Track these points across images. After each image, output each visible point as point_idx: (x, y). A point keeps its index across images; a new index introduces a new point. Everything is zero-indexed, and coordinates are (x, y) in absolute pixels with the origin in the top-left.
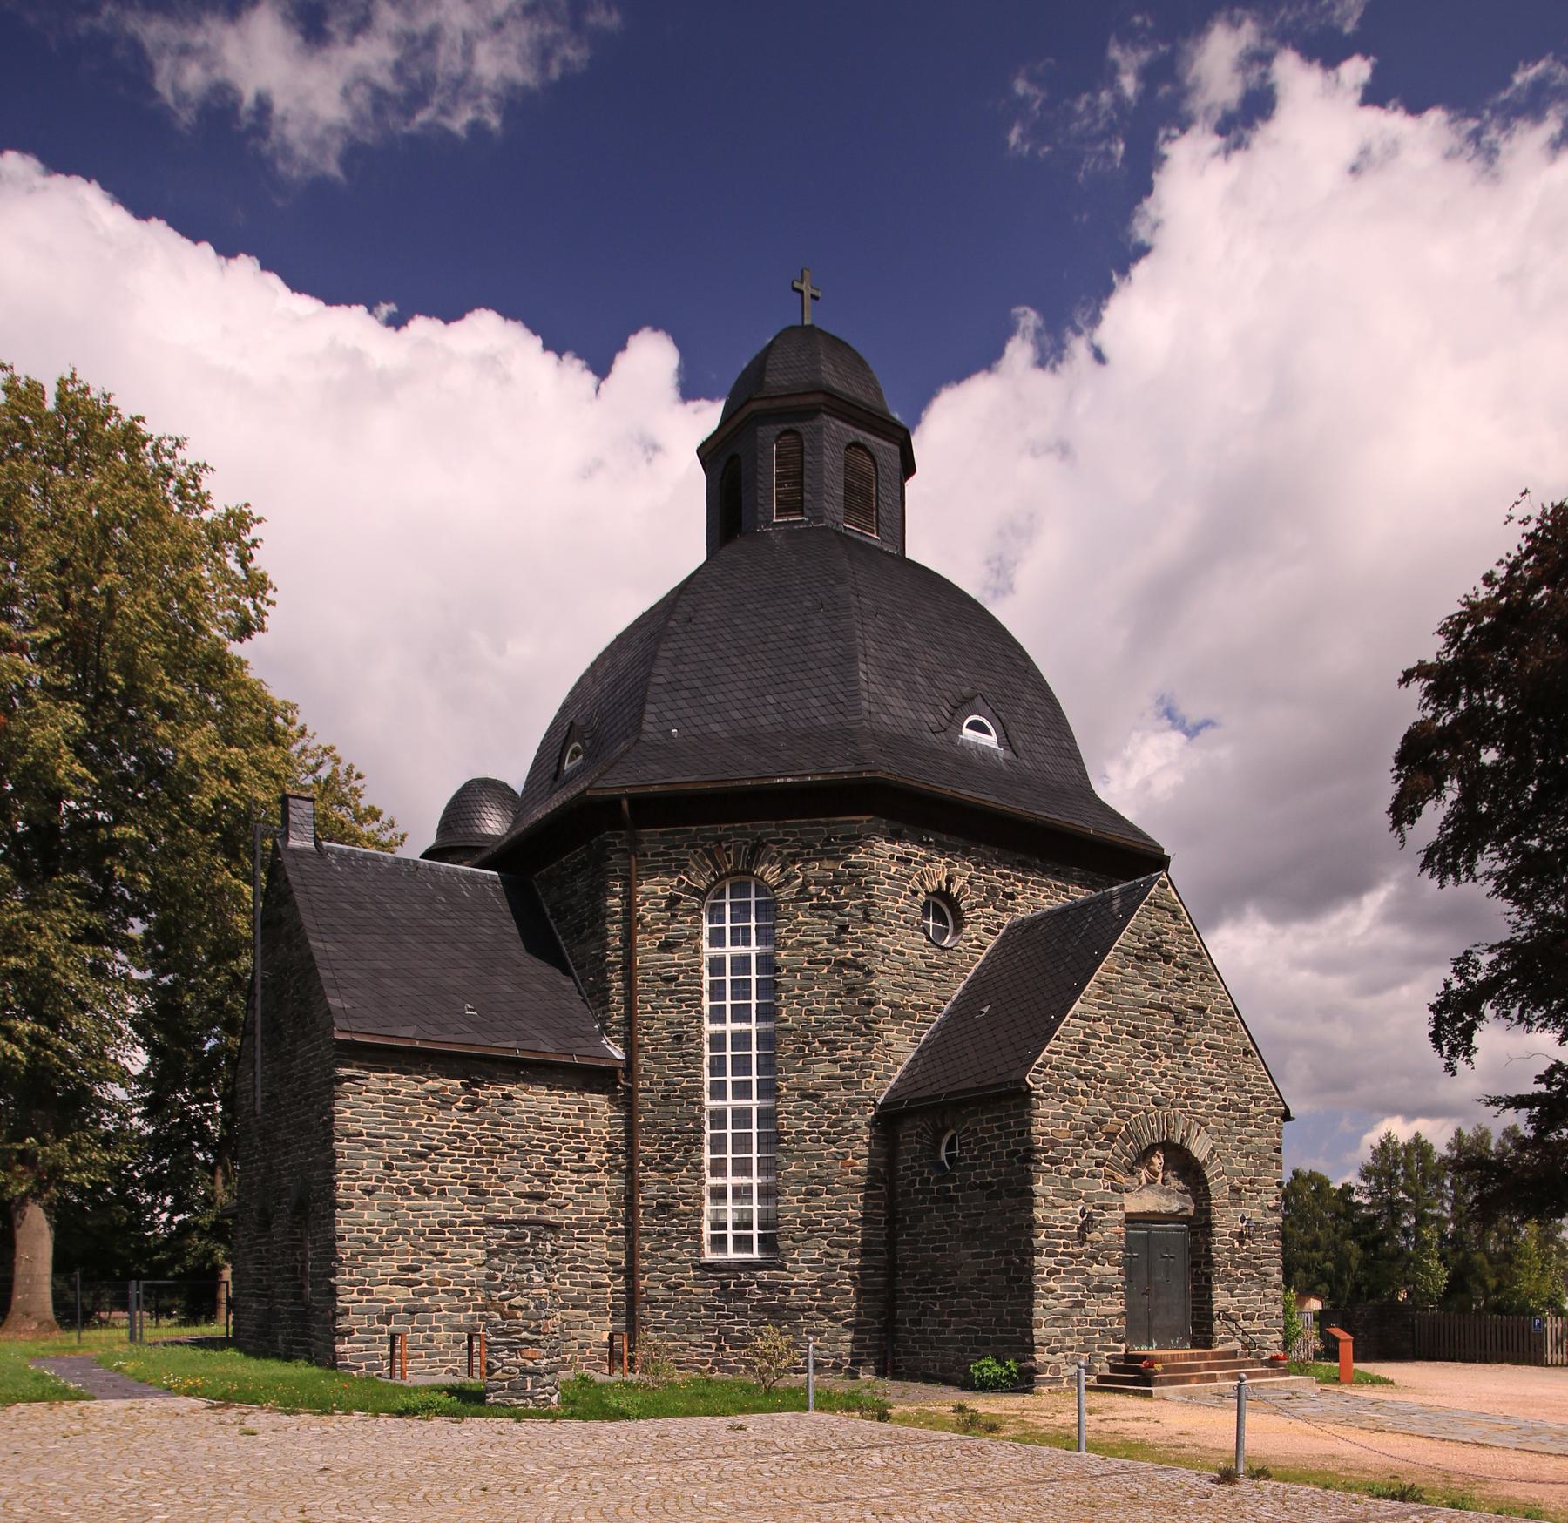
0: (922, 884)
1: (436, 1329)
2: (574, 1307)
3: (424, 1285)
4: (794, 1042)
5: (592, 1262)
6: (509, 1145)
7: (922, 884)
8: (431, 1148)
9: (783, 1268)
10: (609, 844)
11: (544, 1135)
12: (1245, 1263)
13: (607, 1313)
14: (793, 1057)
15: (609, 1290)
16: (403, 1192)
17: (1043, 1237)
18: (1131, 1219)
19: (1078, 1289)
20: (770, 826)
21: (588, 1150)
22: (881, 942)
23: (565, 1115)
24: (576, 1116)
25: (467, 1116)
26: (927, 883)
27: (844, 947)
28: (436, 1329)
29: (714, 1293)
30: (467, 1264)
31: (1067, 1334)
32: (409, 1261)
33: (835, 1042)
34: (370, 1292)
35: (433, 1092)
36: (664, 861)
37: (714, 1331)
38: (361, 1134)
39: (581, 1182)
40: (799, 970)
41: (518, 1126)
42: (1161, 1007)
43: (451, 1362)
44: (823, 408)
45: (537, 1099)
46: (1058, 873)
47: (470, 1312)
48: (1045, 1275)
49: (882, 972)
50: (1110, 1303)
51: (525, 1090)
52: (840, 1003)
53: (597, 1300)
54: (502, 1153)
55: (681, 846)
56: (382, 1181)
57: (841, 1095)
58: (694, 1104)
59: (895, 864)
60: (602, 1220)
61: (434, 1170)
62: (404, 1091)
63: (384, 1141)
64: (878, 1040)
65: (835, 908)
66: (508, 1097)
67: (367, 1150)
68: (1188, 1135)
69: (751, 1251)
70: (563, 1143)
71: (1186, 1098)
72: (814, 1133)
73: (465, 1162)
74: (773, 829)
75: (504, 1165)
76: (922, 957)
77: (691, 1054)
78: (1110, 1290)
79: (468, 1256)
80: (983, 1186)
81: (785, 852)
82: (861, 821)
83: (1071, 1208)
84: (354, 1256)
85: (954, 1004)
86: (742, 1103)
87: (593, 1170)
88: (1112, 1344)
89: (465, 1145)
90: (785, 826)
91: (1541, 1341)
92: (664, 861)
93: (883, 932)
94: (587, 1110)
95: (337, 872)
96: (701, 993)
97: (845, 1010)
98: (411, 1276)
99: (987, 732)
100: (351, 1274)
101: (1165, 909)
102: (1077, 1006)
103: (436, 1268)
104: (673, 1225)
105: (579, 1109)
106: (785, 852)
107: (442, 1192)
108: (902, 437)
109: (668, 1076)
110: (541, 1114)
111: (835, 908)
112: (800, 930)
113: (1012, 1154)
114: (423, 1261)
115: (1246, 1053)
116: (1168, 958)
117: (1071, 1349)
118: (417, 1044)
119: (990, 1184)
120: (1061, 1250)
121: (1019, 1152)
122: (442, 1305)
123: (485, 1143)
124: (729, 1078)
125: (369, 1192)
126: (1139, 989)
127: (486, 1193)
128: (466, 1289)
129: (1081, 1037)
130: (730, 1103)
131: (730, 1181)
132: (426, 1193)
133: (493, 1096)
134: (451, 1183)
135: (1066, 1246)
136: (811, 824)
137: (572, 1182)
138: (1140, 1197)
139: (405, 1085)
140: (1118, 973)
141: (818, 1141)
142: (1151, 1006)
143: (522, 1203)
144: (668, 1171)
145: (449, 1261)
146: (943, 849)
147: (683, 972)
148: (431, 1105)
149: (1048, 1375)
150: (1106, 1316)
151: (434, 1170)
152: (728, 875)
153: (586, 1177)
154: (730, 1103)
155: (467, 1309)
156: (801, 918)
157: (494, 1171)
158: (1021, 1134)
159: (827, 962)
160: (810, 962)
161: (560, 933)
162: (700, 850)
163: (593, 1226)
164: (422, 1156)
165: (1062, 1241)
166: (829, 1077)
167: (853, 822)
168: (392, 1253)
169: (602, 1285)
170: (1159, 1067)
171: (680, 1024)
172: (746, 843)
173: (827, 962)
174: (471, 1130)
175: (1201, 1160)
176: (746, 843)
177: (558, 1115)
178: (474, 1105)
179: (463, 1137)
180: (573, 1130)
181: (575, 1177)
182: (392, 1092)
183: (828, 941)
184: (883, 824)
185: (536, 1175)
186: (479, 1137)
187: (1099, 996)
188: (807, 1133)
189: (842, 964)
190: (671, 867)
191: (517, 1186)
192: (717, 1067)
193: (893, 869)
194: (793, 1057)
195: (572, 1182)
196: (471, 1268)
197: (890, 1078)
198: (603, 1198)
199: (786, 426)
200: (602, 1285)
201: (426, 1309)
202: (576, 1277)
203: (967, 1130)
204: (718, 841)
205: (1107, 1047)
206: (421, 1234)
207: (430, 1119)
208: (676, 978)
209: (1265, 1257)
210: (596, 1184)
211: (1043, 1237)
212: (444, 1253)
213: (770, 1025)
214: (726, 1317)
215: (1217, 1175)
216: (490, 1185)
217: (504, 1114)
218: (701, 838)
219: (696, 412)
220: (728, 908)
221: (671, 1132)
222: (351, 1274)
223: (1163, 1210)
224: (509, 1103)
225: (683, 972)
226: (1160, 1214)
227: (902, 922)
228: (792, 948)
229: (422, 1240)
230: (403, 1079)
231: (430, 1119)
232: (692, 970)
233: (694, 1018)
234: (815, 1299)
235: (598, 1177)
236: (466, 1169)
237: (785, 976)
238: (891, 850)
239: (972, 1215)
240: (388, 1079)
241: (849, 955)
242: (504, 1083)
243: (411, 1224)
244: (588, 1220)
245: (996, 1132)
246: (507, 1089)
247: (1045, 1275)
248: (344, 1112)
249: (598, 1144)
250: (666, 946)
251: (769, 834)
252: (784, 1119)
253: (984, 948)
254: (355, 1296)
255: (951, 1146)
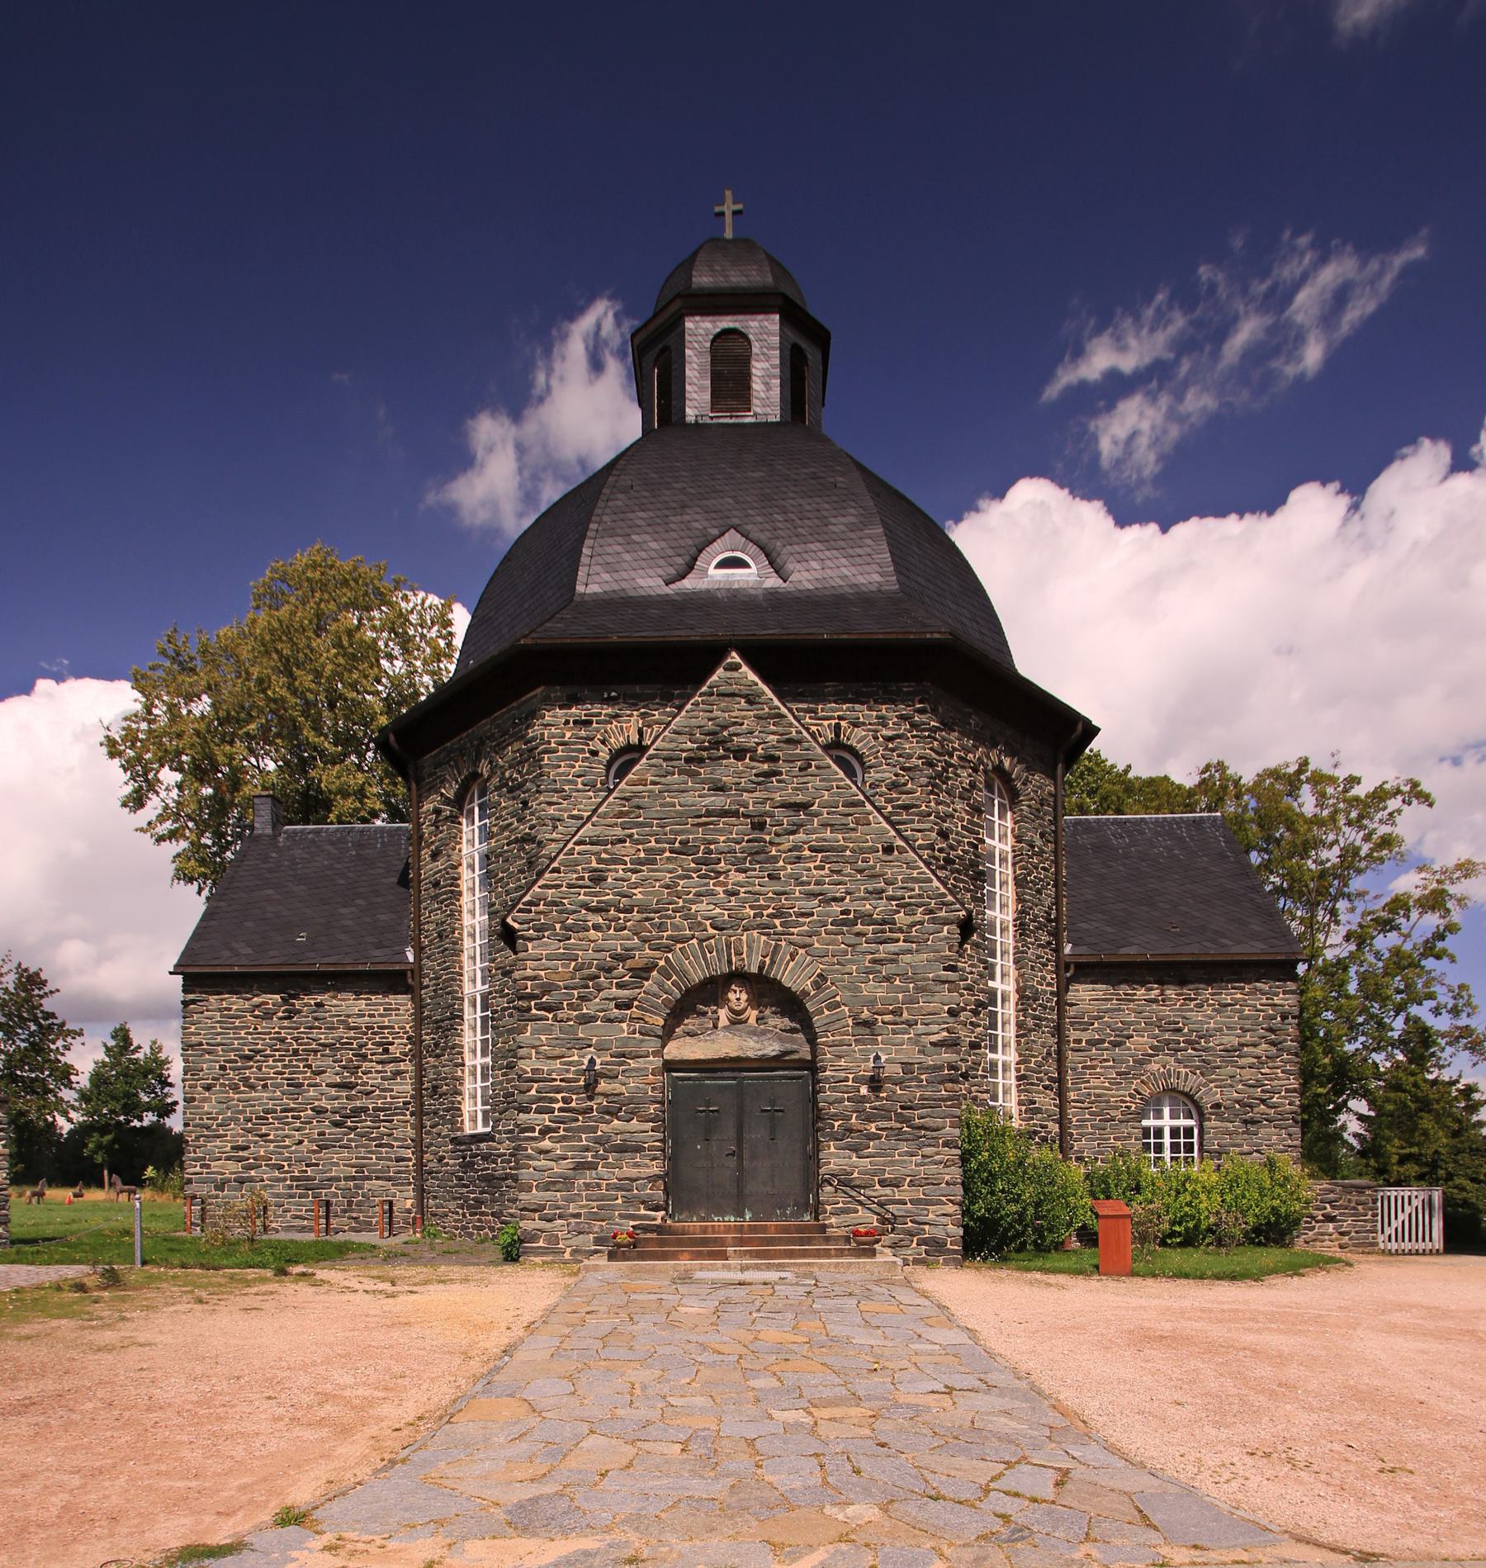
2: (377, 1178)
5: (396, 1139)
6: (320, 1045)
8: (258, 1052)
11: (352, 1034)
12: (883, 1114)
13: (410, 1184)
15: (411, 1164)
16: (235, 1088)
18: (670, 1066)
19: (587, 1149)
20: (485, 725)
21: (393, 1044)
22: (551, 811)
23: (371, 1016)
25: (286, 1023)
31: (570, 1200)
32: (241, 1141)
34: (208, 1166)
35: (258, 1006)
38: (201, 1044)
41: (329, 1028)
42: (725, 813)
44: (683, 311)
45: (349, 1005)
46: (801, 694)
47: (288, 1182)
48: (537, 1134)
49: (553, 840)
50: (636, 1165)
51: (334, 997)
53: (399, 1172)
54: (315, 1052)
56: (218, 1079)
59: (570, 729)
60: (404, 1103)
61: (259, 1068)
62: (235, 1007)
63: (219, 1048)
66: (320, 1005)
67: (207, 1056)
75: (316, 1062)
78: (638, 1149)
79: (287, 1136)
83: (576, 1058)
84: (197, 1138)
88: (643, 1212)
89: (284, 1047)
93: (555, 799)
94: (391, 1009)
98: (241, 1153)
99: (747, 566)
100: (195, 1152)
101: (733, 695)
103: (261, 1146)
105: (385, 1010)
107: (265, 1086)
110: (348, 1016)
114: (251, 1142)
115: (888, 850)
116: (740, 754)
117: (578, 1216)
118: (236, 969)
123: (301, 1044)
125: (208, 1088)
126: (688, 798)
127: (302, 1085)
128: (285, 1164)
129: (594, 865)
132: (252, 1087)
133: (306, 1005)
134: (272, 1078)
135: (565, 1100)
137: (378, 1072)
138: (713, 1041)
139: (235, 1003)
140: (654, 783)
142: (709, 814)
143: (333, 1092)
145: (271, 1141)
146: (633, 701)
148: (256, 1017)
149: (541, 1244)
150: (633, 1180)
151: (259, 1068)
153: (390, 1068)
155: (285, 1179)
157: (310, 1067)
163: (396, 1108)
164: (249, 1058)
167: (528, 700)
168: (226, 1136)
169: (404, 1159)
170: (724, 884)
174: (289, 1034)
177: (364, 1016)
179: (283, 1040)
181: (379, 1068)
182: (226, 1009)
184: (557, 692)
185: (344, 1067)
186: (296, 1039)
187: (621, 815)
191: (330, 1077)
193: (568, 734)
195: (378, 1072)
196: (290, 1147)
198: (407, 1084)
199: (660, 346)
200: (404, 1159)
201: (251, 1180)
202: (381, 1153)
205: (634, 871)
206: (250, 1120)
207: (256, 1029)
210: (398, 1073)
212: (268, 1135)
216: (305, 1079)
217: (316, 1019)
219: (561, 379)
222: (195, 1152)
223: (751, 1054)
224: (321, 1009)
226: (748, 1059)
227: (580, 786)
229: (250, 1125)
230: (234, 998)
231: (256, 1029)
235: (402, 1066)
236: (285, 1066)
238: (566, 715)
240: (222, 1000)
242: (317, 994)
243: (241, 1112)
244: (392, 1103)
246: (319, 998)
247: (537, 1134)
249: (402, 1038)
254: (198, 1169)
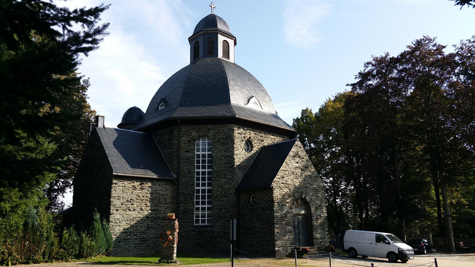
0: (244, 139)
1: (131, 244)
3: (129, 233)
4: (216, 174)
7: (244, 139)
9: (213, 227)
10: (174, 129)
11: (157, 195)
14: (216, 177)
17: (276, 220)
21: (167, 199)
23: (163, 191)
24: (165, 191)
26: (245, 139)
27: (228, 153)
28: (131, 244)
29: (196, 234)
30: (139, 228)
33: (226, 174)
36: (187, 133)
37: (196, 243)
39: (165, 207)
40: (218, 158)
43: (134, 252)
52: (227, 165)
55: (191, 130)
57: (227, 186)
58: (193, 188)
64: (236, 174)
65: (226, 144)
68: (306, 196)
69: (205, 223)
70: (161, 197)
71: (305, 187)
72: (221, 195)
73: (140, 203)
74: (212, 127)
76: (245, 155)
77: (192, 176)
80: (262, 208)
81: (215, 132)
82: (232, 126)
85: (251, 165)
86: (204, 188)
87: (168, 204)
90: (215, 126)
91: (123, 131)
92: (187, 133)
95: (109, 133)
96: (195, 162)
97: (228, 167)
102: (281, 168)
104: (187, 217)
105: (166, 189)
106: (215, 132)
108: (234, 39)
109: (187, 181)
110: (157, 191)
111: (226, 144)
112: (218, 149)
113: (268, 201)
119: (263, 208)
120: (280, 223)
121: (270, 200)
122: (132, 238)
124: (201, 182)
128: (138, 234)
130: (201, 188)
131: (200, 206)
132: (130, 210)
136: (220, 126)
137: (163, 207)
139: (126, 183)
141: (222, 196)
144: (186, 204)
147: (191, 158)
148: (132, 189)
152: (201, 136)
153: (166, 205)
154: (201, 188)
155: (138, 239)
156: (218, 146)
158: (271, 196)
159: (224, 156)
160: (220, 156)
161: (159, 147)
162: (195, 131)
165: (280, 221)
166: (225, 182)
171: (190, 170)
172: (206, 130)
173: (224, 156)
175: (309, 201)
176: (206, 130)
177: (161, 191)
178: (142, 189)
179: (139, 196)
180: (164, 194)
181: (164, 205)
183: (224, 152)
188: (219, 195)
189: (228, 156)
190: (188, 134)
192: (198, 179)
194: (216, 177)
195: (163, 207)
196: (140, 229)
197: (238, 182)
201: (129, 239)
203: (257, 195)
204: (199, 129)
208: (189, 159)
209: (324, 224)
211: (276, 220)
213: (211, 170)
214: (200, 239)
215: (312, 205)
218: (195, 128)
220: (201, 143)
221: (187, 194)
225: (191, 158)
228: (216, 153)
232: (193, 157)
233: (193, 168)
234: (221, 235)
237: (214, 159)
239: (259, 215)
241: (229, 155)
245: (264, 196)
248: (113, 191)
249: (169, 197)
250: (187, 151)
251: (210, 128)
252: (214, 192)
253: (258, 152)
255: (253, 198)
